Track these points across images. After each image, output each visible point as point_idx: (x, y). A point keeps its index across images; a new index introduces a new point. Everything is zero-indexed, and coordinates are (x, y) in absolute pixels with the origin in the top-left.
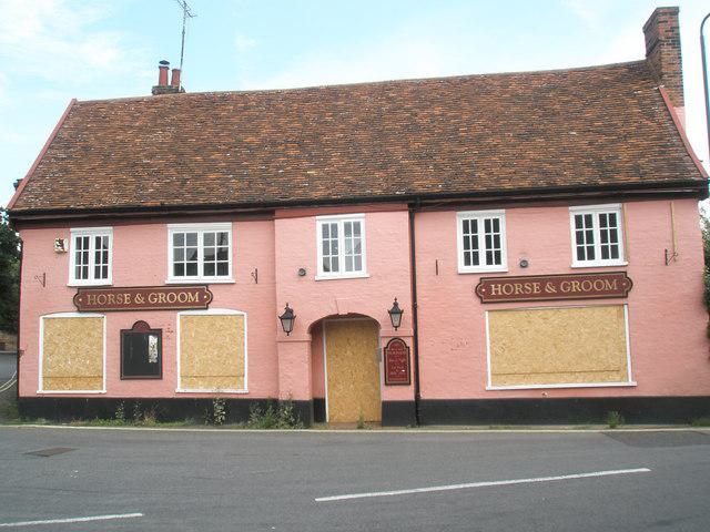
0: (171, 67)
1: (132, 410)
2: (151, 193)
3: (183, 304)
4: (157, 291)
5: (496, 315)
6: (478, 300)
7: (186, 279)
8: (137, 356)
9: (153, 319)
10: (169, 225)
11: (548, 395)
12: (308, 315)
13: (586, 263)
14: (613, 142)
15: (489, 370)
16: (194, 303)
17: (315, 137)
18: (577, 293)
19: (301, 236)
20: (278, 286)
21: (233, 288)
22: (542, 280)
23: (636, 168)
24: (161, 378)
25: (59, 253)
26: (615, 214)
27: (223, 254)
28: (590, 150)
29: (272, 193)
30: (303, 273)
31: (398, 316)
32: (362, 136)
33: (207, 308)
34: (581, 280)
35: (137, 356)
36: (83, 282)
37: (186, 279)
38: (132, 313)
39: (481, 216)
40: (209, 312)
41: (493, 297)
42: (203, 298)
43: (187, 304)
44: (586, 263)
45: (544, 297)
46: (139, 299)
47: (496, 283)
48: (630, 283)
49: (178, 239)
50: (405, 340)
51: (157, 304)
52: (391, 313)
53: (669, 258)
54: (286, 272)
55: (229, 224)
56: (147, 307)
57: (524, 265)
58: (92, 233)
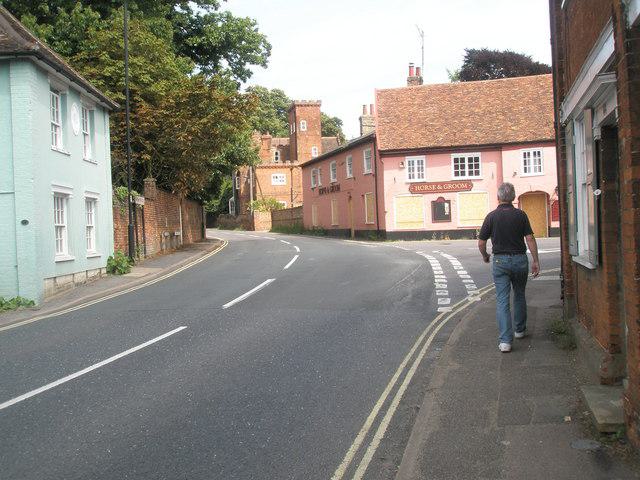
1: (439, 235)
2: (441, 140)
7: (460, 178)
8: (439, 211)
9: (446, 196)
17: (510, 109)
19: (512, 158)
27: (456, 167)
29: (499, 139)
32: (533, 108)
35: (439, 211)
36: (412, 181)
37: (460, 178)
42: (468, 186)
46: (439, 187)
49: (456, 160)
52: (601, 458)
58: (416, 158)
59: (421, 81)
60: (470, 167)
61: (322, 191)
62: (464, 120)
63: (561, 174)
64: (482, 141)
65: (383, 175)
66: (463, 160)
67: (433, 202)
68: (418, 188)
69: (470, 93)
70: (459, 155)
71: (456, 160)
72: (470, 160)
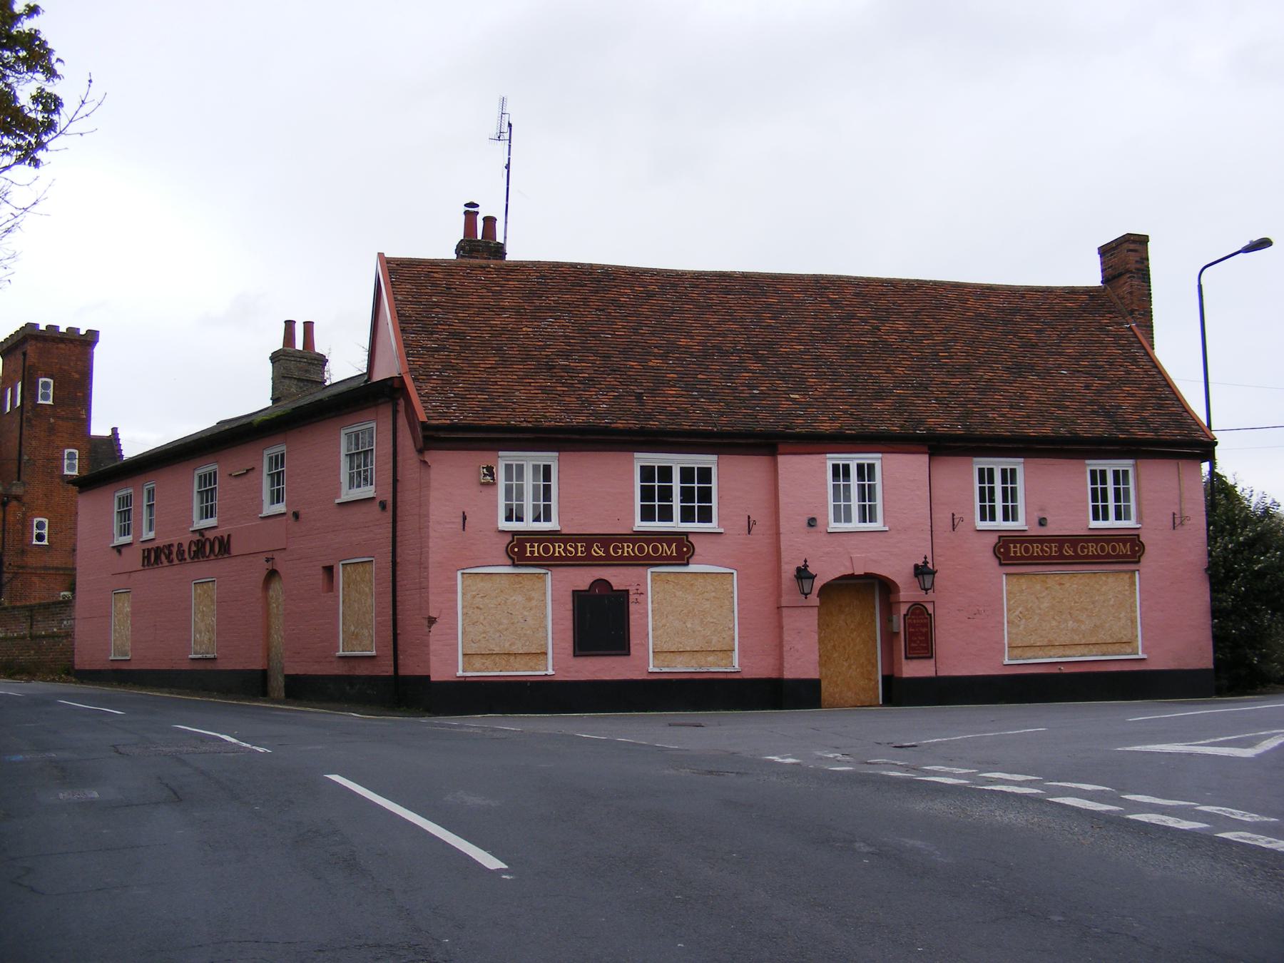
0: (483, 213)
3: (655, 559)
4: (622, 541)
5: (1015, 579)
6: (997, 562)
7: (656, 526)
10: (637, 455)
11: (1064, 669)
12: (826, 572)
13: (1100, 524)
14: (1108, 387)
15: (1006, 642)
16: (670, 558)
18: (1093, 557)
20: (782, 537)
21: (722, 536)
22: (1061, 540)
23: (1144, 422)
24: (628, 654)
25: (487, 484)
26: (1127, 471)
27: (647, 494)
28: (1090, 395)
29: (765, 421)
30: (812, 522)
31: (932, 576)
33: (687, 564)
34: (634, 542)
36: (514, 526)
37: (656, 526)
38: (588, 569)
39: (998, 465)
40: (692, 568)
41: (1012, 558)
42: (682, 549)
43: (661, 558)
44: (1100, 524)
45: (1061, 560)
46: (597, 551)
47: (1015, 542)
48: (1142, 546)
49: (647, 473)
50: (927, 605)
51: (621, 557)
53: (1177, 521)
54: (791, 522)
55: (714, 458)
56: (608, 561)
57: (1042, 522)
58: (530, 460)
59: (500, 251)
60: (687, 494)
61: (155, 556)
62: (654, 363)
63: (551, 533)
64: (724, 423)
65: (424, 516)
66: (666, 473)
67: (577, 595)
68: (536, 550)
69: (650, 295)
70: (657, 459)
71: (647, 473)
72: (687, 474)
